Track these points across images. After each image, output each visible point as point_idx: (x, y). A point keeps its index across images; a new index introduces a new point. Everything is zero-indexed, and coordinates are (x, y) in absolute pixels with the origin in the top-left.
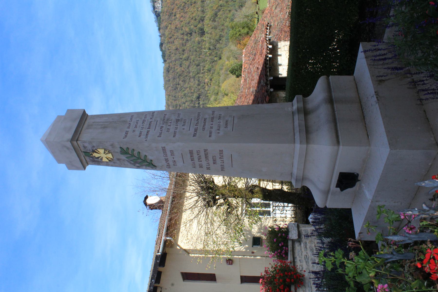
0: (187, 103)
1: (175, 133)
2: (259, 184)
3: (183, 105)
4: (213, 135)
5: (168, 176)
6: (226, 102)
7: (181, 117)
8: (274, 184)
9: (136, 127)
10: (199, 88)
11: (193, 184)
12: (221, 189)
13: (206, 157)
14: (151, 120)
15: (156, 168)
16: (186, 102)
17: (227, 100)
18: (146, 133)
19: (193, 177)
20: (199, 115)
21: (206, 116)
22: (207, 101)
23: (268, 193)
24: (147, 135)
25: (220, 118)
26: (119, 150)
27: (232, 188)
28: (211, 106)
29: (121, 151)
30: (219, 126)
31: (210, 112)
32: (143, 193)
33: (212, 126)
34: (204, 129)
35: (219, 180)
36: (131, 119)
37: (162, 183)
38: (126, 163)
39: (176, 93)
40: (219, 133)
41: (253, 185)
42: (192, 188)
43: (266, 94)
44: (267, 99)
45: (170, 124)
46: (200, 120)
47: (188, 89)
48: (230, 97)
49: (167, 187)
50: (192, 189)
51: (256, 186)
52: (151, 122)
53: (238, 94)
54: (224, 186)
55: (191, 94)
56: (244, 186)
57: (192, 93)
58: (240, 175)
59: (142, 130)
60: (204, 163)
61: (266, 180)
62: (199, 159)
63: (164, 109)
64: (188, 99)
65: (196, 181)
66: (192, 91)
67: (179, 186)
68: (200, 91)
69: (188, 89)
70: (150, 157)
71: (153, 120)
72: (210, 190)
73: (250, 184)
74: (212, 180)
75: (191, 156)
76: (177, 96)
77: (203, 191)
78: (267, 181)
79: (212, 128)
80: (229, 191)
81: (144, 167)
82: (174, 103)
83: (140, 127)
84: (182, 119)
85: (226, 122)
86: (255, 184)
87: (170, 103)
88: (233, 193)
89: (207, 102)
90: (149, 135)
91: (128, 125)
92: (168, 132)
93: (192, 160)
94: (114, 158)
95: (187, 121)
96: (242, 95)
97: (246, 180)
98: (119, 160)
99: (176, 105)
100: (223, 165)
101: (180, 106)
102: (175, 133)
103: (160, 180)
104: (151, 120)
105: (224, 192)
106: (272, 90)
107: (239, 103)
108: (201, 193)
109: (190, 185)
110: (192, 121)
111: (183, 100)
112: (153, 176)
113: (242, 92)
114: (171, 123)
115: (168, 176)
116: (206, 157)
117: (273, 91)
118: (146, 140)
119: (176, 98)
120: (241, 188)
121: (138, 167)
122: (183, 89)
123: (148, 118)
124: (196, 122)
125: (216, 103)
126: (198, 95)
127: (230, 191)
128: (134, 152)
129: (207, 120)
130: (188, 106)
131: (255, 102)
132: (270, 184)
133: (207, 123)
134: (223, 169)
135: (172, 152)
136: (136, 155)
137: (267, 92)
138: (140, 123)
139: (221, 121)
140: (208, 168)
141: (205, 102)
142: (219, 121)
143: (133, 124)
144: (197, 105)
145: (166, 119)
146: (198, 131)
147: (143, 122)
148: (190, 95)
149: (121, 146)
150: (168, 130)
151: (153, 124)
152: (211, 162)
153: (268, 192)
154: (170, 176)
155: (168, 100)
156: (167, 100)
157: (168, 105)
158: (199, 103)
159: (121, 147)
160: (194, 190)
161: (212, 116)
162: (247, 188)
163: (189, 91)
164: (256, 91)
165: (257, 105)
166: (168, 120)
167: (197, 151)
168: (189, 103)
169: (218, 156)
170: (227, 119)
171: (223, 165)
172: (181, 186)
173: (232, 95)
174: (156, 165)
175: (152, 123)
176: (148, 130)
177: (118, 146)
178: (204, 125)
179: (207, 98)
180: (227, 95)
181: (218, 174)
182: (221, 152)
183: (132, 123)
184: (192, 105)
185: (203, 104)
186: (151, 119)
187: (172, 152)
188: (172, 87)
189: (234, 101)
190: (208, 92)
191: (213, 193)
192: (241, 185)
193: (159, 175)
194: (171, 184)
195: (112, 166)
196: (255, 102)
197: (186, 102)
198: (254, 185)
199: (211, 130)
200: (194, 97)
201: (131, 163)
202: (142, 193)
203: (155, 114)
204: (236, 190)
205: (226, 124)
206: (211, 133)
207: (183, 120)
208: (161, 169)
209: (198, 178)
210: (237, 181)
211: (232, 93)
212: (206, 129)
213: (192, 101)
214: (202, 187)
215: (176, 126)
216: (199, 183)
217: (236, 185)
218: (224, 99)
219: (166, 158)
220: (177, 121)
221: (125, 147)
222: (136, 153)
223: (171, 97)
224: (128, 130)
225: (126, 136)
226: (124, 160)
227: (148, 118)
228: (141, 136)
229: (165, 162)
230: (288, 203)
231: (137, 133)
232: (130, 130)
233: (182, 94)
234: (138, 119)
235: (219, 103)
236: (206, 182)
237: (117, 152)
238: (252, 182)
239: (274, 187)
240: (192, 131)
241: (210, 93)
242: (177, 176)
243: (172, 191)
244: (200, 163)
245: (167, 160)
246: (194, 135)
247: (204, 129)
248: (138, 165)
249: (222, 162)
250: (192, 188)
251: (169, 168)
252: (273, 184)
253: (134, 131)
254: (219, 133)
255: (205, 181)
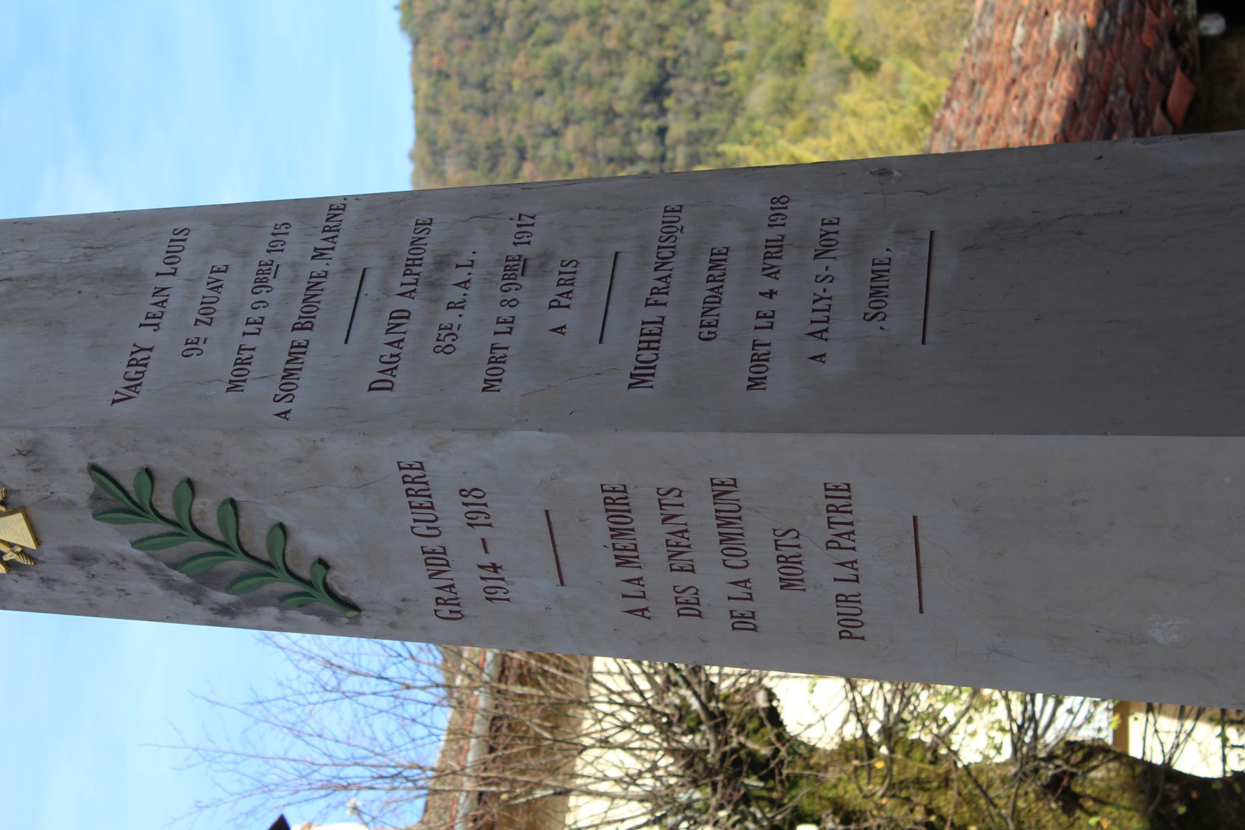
0: (570, 134)
1: (497, 361)
2: (1121, 733)
3: (547, 148)
4: (778, 369)
5: (439, 678)
6: (865, 125)
7: (540, 236)
8: (1231, 732)
9: (207, 315)
10: (664, 18)
11: (624, 736)
12: (832, 775)
13: (730, 540)
14: (319, 266)
15: (355, 622)
16: (566, 121)
17: (871, 108)
18: (280, 367)
19: (620, 684)
20: (670, 229)
21: (729, 235)
22: (723, 116)
23: (1191, 804)
24: (288, 373)
25: (825, 249)
26: (85, 486)
27: (915, 766)
28: (754, 157)
29: (96, 498)
30: (823, 309)
31: (757, 203)
32: (257, 800)
33: (766, 305)
34: (709, 330)
35: (816, 709)
36: (172, 257)
37: (392, 725)
38: (137, 582)
39: (492, 56)
40: (819, 358)
41: (1071, 746)
42: (615, 762)
43: (1166, 55)
44: (1178, 96)
45: (456, 294)
46: (678, 266)
47: (580, 26)
48: (896, 80)
49: (433, 755)
50: (618, 774)
51: (1093, 751)
52: (315, 283)
53: (954, 60)
54: (858, 752)
55: (605, 67)
56: (1007, 752)
57: (606, 54)
58: (975, 671)
59: (250, 341)
60: (712, 580)
61: (1174, 708)
62: (677, 550)
63: (396, 175)
64: (583, 100)
65: (649, 713)
66: (611, 43)
67: (521, 747)
68: (670, 39)
69: (580, 26)
70: (311, 542)
71: (334, 267)
72: (753, 782)
73: (1050, 737)
74: (761, 700)
75: (616, 533)
76: (497, 82)
77: (695, 783)
78: (1182, 715)
79: (767, 319)
80: (894, 788)
81: (271, 612)
82: (480, 133)
83: (234, 314)
84: (546, 256)
85: (877, 275)
86: (1086, 734)
87: (445, 133)
88: (921, 798)
89: (716, 119)
90: (304, 379)
91: (146, 304)
92: (447, 350)
93: (622, 562)
94: (48, 552)
95: (584, 274)
96: (988, 71)
97: (1017, 709)
98: (79, 558)
99: (495, 153)
100: (855, 599)
101: (522, 155)
102: (497, 361)
103: (383, 702)
104: (319, 266)
105: (851, 793)
106: (1213, 25)
107: (961, 132)
108: (683, 797)
109: (605, 743)
110: (623, 274)
111: (547, 110)
112: (326, 675)
113: (983, 45)
114: (464, 284)
115: (439, 678)
116: (730, 540)
117: (1225, 36)
118: (284, 414)
119: (489, 98)
120: (980, 768)
121: (226, 615)
122: (546, 29)
123: (297, 248)
124: (650, 279)
125: (793, 126)
126: (650, 72)
127: (903, 784)
128: (198, 505)
129: (734, 265)
130: (582, 151)
131: (1084, 120)
132: (1206, 732)
133: (730, 288)
134: (850, 628)
135: (476, 507)
136: (210, 525)
137: (1176, 40)
138: (237, 289)
139: (837, 268)
140: (744, 622)
141: (704, 122)
142: (819, 267)
143: (183, 300)
144: (646, 148)
145: (428, 258)
146: (666, 345)
147: (261, 283)
148: (594, 68)
149: (100, 461)
150: (446, 339)
151: (337, 293)
152: (764, 574)
153: (1184, 798)
154: (450, 672)
155: (434, 111)
156: (427, 110)
157: (430, 149)
158: (662, 132)
159: (94, 468)
160: (633, 779)
161: (773, 234)
162: (1028, 759)
163: (590, 42)
164: (1091, 33)
165: (1097, 146)
166: (442, 263)
167: (662, 495)
168: (587, 128)
169: (815, 531)
170: (882, 254)
171: (855, 599)
172: (535, 752)
173: (910, 68)
174: (355, 597)
175: (328, 285)
176: (301, 336)
177: (71, 457)
178: (713, 302)
179: (724, 94)
180: (870, 67)
181: (814, 664)
182: (838, 498)
183: (177, 288)
184: (611, 144)
185: (693, 139)
186: (319, 254)
187: (476, 507)
188: (464, 15)
189: (924, 110)
190: (732, 47)
191: (774, 804)
192: (981, 742)
193: (375, 667)
194: (457, 734)
195: (28, 605)
196: (1084, 120)
197: (566, 121)
198: (1081, 745)
199: (763, 336)
200: (627, 85)
201: (169, 585)
202: (245, 805)
203: (349, 219)
204: (946, 782)
205: (876, 293)
206: (759, 360)
207: (555, 265)
208: (395, 625)
209: (661, 691)
210: (950, 712)
211: (911, 50)
212: (725, 328)
213: (611, 115)
214: (690, 757)
215: (506, 312)
216: (665, 730)
217: (943, 739)
218: (848, 100)
219: (431, 544)
220: (515, 269)
221: (125, 468)
222: (206, 511)
223: (452, 85)
224: (146, 337)
225: (134, 385)
226: (118, 563)
227: (297, 248)
228: (251, 387)
229: (422, 573)
230: (958, 684)
231: (218, 359)
232: (165, 340)
233: (539, 65)
234: (219, 259)
235: (812, 128)
236: (719, 721)
237: (70, 505)
238: (1062, 720)
239: (1232, 755)
240: (623, 342)
241: (740, 56)
242: (502, 675)
243: (468, 785)
244: (685, 579)
245: (436, 561)
246: (640, 378)
247: (709, 330)
248: (223, 598)
249: (845, 573)
250: (615, 762)
251: (457, 616)
252: (1225, 740)
253: (192, 347)
254: (819, 358)
255: (711, 715)
